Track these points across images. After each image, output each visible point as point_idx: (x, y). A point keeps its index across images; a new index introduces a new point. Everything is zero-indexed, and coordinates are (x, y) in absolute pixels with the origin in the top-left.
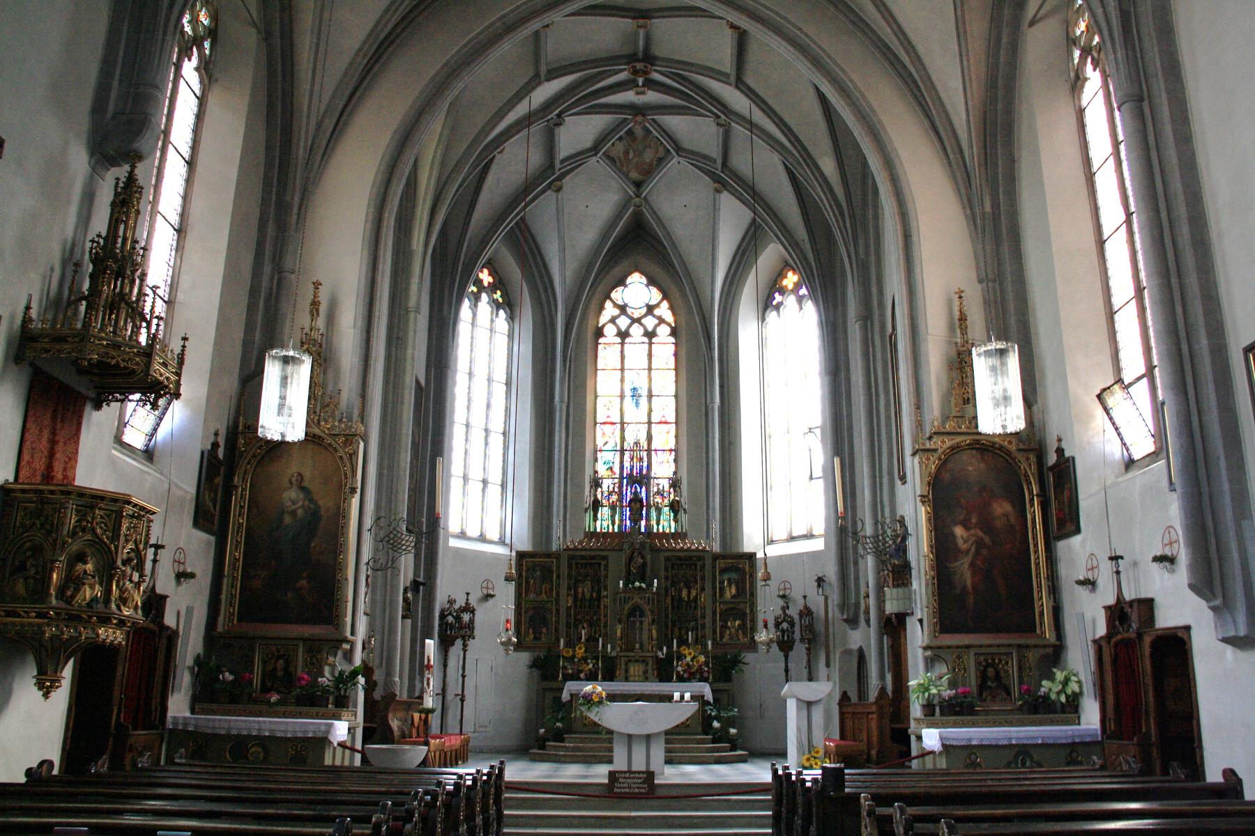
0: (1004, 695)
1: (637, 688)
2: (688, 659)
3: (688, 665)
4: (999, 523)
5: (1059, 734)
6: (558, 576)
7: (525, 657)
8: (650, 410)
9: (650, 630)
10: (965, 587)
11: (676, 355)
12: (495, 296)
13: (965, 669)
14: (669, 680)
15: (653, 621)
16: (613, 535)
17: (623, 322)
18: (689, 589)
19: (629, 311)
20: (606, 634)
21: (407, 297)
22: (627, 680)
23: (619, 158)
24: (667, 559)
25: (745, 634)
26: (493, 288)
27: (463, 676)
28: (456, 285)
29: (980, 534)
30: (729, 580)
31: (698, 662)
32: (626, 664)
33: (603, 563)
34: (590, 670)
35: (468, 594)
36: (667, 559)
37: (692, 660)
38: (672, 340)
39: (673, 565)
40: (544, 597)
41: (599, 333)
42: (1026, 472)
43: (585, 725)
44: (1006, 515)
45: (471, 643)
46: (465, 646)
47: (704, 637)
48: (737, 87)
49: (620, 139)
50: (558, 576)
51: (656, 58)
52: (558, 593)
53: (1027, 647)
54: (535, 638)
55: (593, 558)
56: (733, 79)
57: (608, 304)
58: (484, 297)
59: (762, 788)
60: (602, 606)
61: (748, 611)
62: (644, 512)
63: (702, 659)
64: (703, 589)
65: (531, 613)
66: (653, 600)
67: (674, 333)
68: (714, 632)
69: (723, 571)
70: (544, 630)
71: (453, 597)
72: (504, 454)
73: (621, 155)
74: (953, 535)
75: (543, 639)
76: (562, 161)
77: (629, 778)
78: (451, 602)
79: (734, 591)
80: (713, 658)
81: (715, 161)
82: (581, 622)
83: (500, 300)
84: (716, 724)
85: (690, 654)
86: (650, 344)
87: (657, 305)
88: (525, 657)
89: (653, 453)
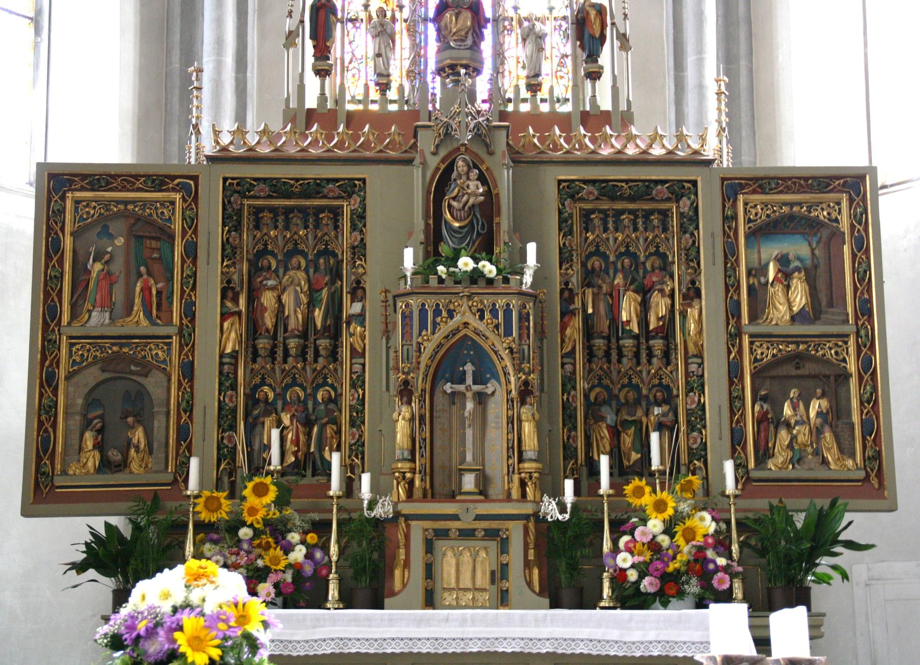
1: (470, 631)
2: (655, 525)
3: (653, 546)
9: (514, 423)
15: (525, 392)
16: (381, 121)
18: (645, 292)
20: (357, 450)
22: (430, 601)
24: (568, 190)
25: (846, 450)
30: (783, 261)
31: (689, 535)
32: (429, 547)
33: (347, 208)
34: (297, 568)
36: (568, 190)
37: (669, 530)
39: (586, 216)
40: (139, 323)
47: (700, 453)
50: (191, 252)
52: (189, 312)
54: (106, 465)
55: (315, 188)
60: (345, 353)
61: (852, 366)
62: (486, 46)
63: (706, 524)
64: (693, 293)
65: (93, 375)
66: (523, 318)
68: (737, 440)
69: (759, 233)
70: (139, 435)
75: (134, 466)
79: (799, 297)
82: (270, 408)
85: (660, 506)
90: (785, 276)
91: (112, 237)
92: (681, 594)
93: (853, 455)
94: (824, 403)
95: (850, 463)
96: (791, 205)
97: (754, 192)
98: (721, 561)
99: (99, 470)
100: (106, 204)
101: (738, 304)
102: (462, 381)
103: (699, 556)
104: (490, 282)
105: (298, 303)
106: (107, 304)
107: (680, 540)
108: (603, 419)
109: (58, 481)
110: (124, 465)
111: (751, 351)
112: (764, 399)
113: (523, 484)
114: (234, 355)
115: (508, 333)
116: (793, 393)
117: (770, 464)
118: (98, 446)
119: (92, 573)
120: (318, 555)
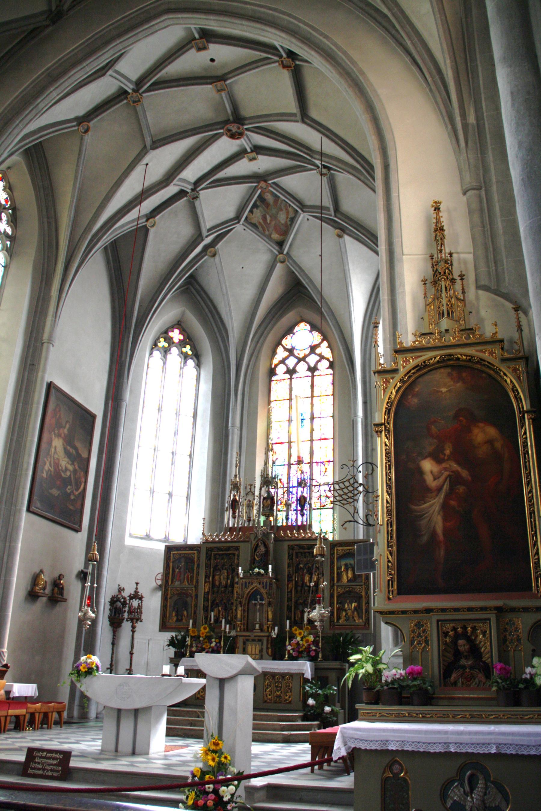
0: (481, 676)
2: (299, 639)
4: (482, 451)
5: (525, 741)
6: (198, 565)
7: (168, 636)
8: (312, 430)
10: (434, 533)
11: (333, 383)
12: (184, 350)
13: (426, 642)
14: (282, 658)
17: (291, 362)
19: (296, 353)
21: (43, 333)
23: (260, 223)
24: (291, 548)
25: (360, 617)
26: (182, 344)
27: (131, 654)
28: (131, 336)
29: (455, 466)
30: (346, 565)
32: (244, 643)
33: (236, 553)
35: (137, 584)
37: (302, 640)
38: (330, 371)
39: (297, 553)
41: (272, 372)
42: (514, 386)
43: (266, 702)
44: (490, 442)
45: (138, 625)
46: (133, 627)
48: (303, 122)
49: (255, 206)
50: (198, 565)
51: (245, 119)
52: (197, 582)
53: (513, 610)
55: (228, 549)
56: (299, 117)
57: (280, 349)
58: (174, 351)
59: (168, 783)
61: (363, 594)
63: (311, 638)
65: (176, 598)
67: (332, 365)
69: (340, 558)
70: (185, 613)
71: (122, 586)
72: (189, 471)
73: (261, 221)
74: (420, 472)
75: (184, 621)
76: (209, 230)
77: (45, 758)
78: (121, 590)
80: (323, 638)
81: (328, 209)
83: (190, 353)
84: (311, 702)
85: (300, 634)
86: (313, 376)
87: (318, 346)
88: (168, 636)
89: (314, 465)
90: (347, 569)
91: (181, 563)
92: (302, 657)
93: (362, 619)
94: (356, 604)
95: (361, 620)
96: (349, 549)
97: (339, 547)
98: (314, 648)
99: (176, 621)
100: (180, 554)
101: (333, 577)
102: (257, 600)
103: (309, 647)
104: (263, 575)
105: (224, 579)
106: (179, 580)
107: (304, 643)
108: (298, 609)
109: (167, 624)
110: (182, 620)
111: (337, 590)
112: (340, 603)
113: (268, 628)
114: (208, 592)
115: (266, 588)
116: (348, 601)
117: (340, 621)
118: (177, 615)
119: (171, 647)
120: (218, 645)
